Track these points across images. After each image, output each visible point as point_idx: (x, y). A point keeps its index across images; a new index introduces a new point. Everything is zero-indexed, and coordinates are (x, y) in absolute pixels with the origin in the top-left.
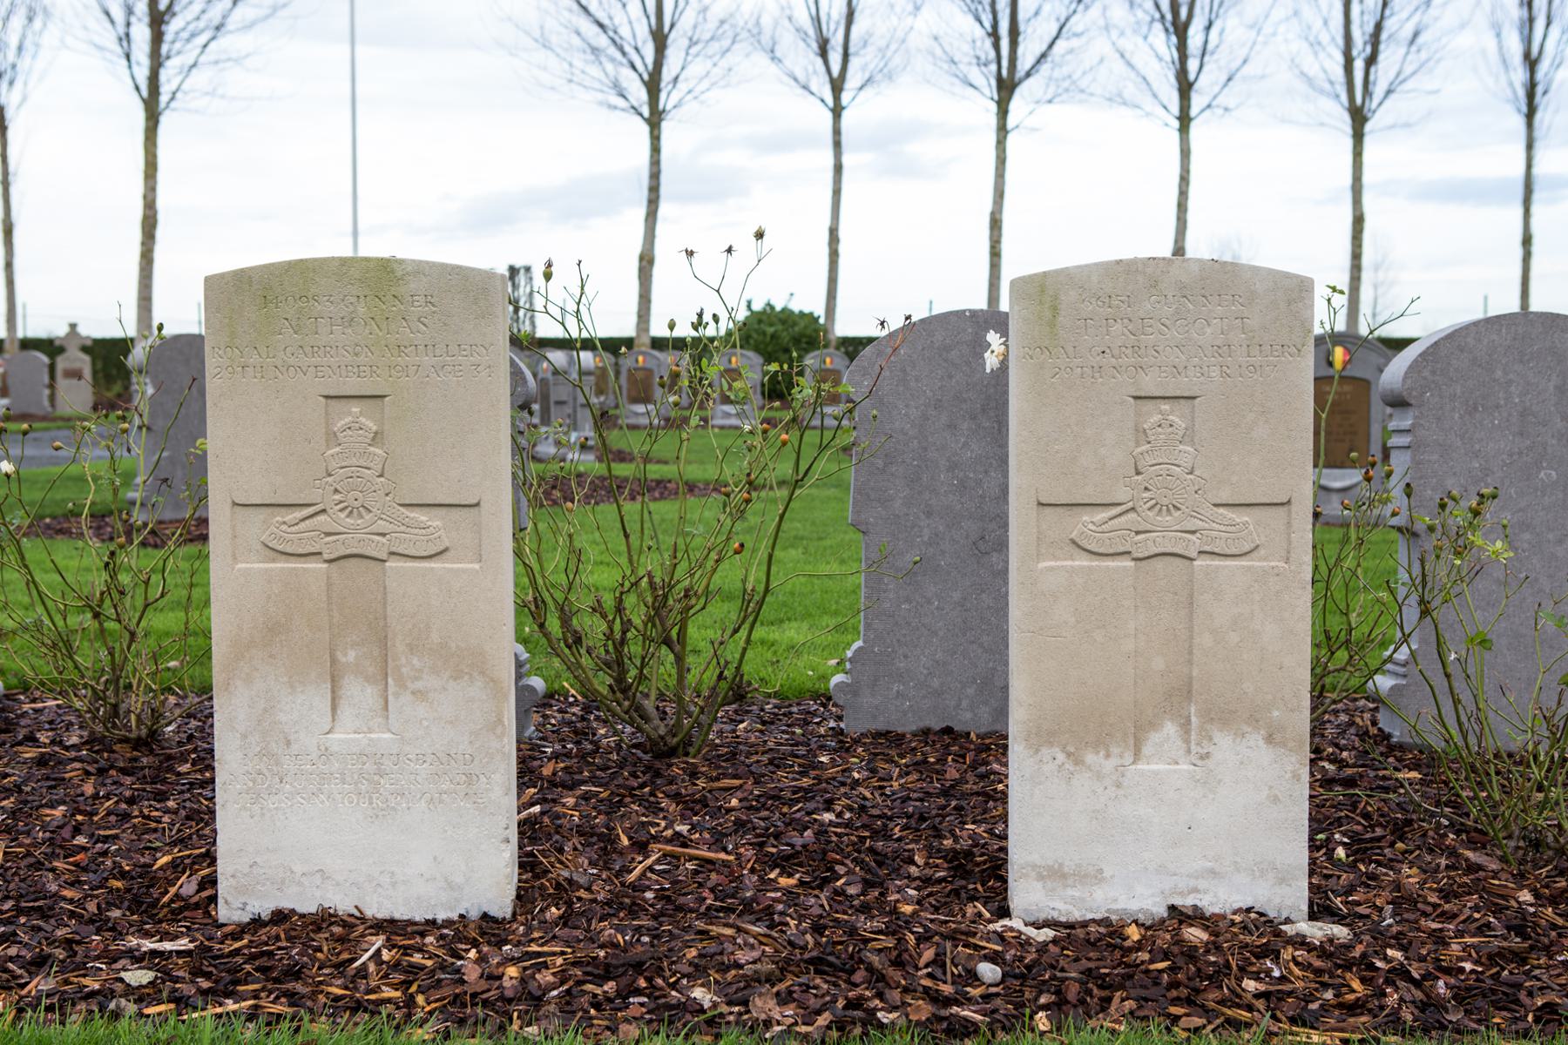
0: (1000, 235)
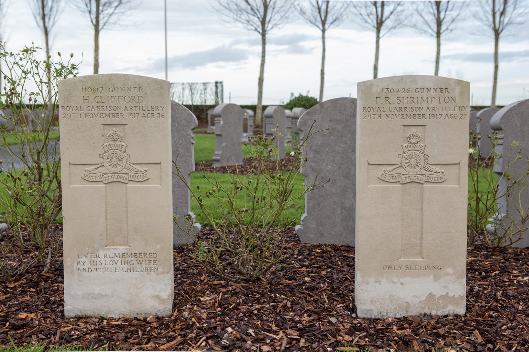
0: (377, 72)
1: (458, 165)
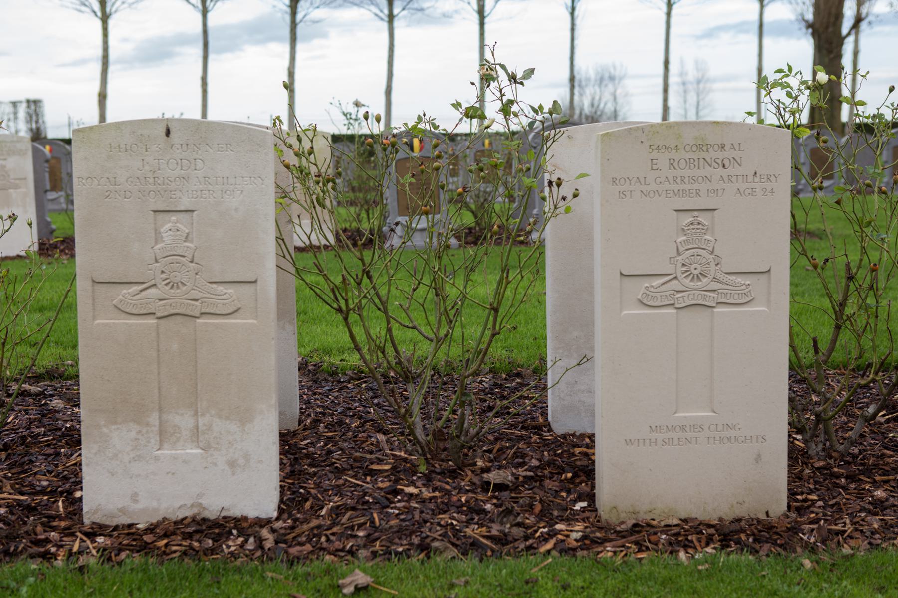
0: (289, 111)
1: (765, 275)
